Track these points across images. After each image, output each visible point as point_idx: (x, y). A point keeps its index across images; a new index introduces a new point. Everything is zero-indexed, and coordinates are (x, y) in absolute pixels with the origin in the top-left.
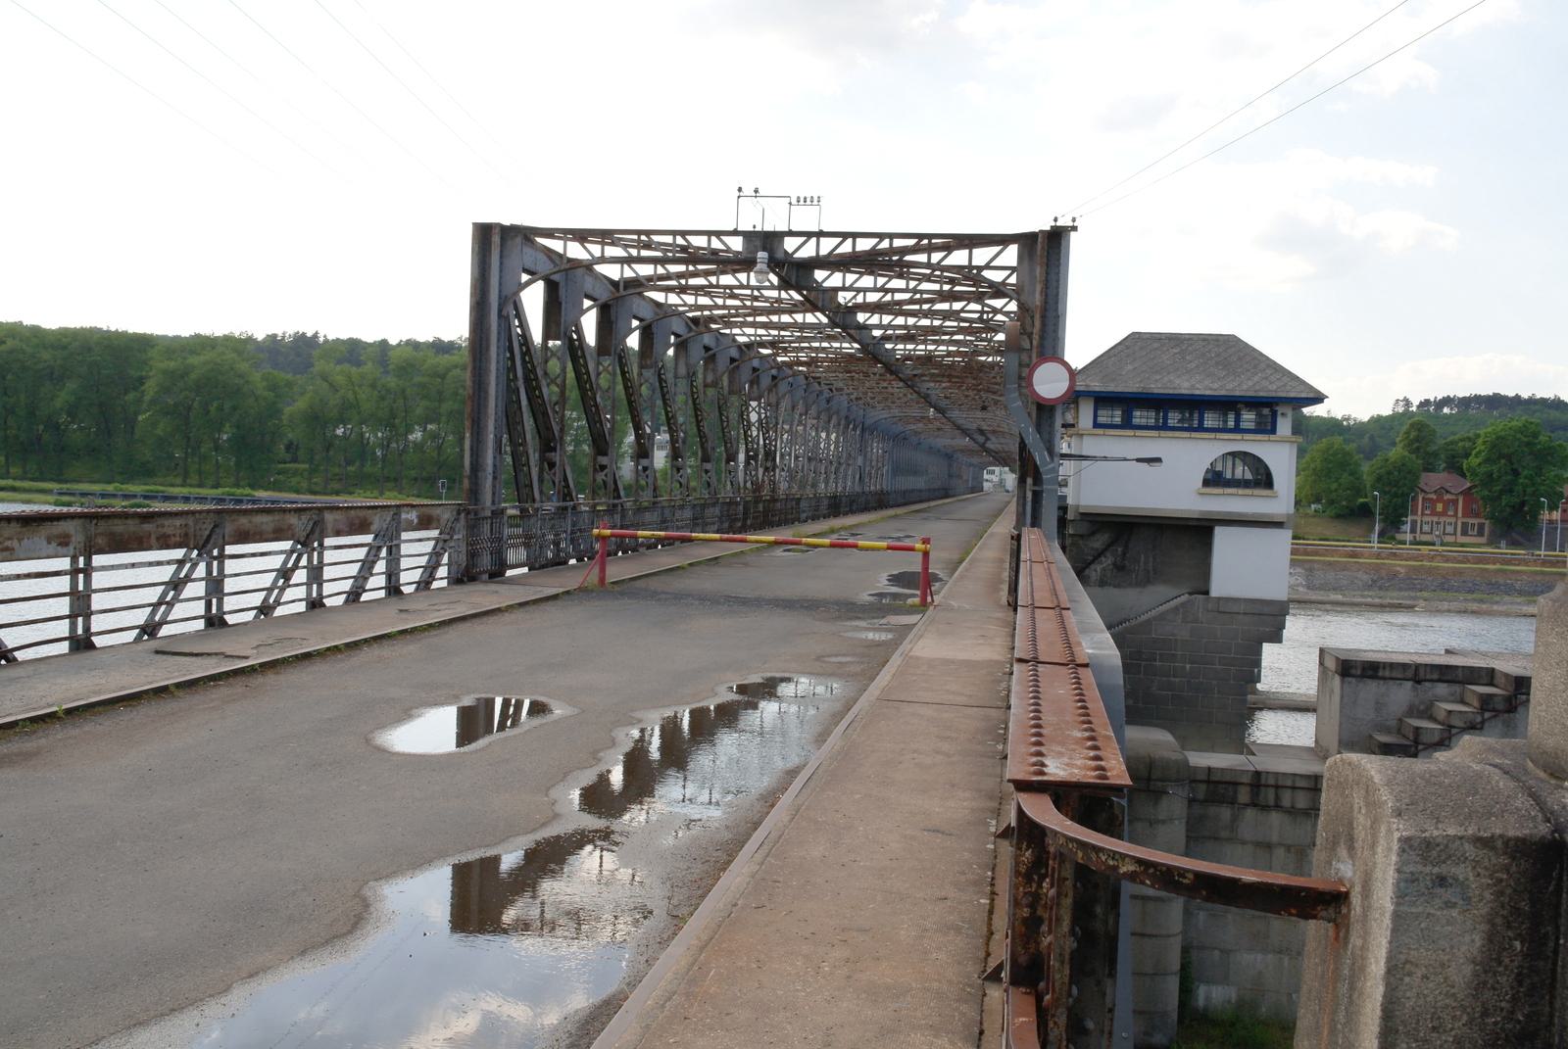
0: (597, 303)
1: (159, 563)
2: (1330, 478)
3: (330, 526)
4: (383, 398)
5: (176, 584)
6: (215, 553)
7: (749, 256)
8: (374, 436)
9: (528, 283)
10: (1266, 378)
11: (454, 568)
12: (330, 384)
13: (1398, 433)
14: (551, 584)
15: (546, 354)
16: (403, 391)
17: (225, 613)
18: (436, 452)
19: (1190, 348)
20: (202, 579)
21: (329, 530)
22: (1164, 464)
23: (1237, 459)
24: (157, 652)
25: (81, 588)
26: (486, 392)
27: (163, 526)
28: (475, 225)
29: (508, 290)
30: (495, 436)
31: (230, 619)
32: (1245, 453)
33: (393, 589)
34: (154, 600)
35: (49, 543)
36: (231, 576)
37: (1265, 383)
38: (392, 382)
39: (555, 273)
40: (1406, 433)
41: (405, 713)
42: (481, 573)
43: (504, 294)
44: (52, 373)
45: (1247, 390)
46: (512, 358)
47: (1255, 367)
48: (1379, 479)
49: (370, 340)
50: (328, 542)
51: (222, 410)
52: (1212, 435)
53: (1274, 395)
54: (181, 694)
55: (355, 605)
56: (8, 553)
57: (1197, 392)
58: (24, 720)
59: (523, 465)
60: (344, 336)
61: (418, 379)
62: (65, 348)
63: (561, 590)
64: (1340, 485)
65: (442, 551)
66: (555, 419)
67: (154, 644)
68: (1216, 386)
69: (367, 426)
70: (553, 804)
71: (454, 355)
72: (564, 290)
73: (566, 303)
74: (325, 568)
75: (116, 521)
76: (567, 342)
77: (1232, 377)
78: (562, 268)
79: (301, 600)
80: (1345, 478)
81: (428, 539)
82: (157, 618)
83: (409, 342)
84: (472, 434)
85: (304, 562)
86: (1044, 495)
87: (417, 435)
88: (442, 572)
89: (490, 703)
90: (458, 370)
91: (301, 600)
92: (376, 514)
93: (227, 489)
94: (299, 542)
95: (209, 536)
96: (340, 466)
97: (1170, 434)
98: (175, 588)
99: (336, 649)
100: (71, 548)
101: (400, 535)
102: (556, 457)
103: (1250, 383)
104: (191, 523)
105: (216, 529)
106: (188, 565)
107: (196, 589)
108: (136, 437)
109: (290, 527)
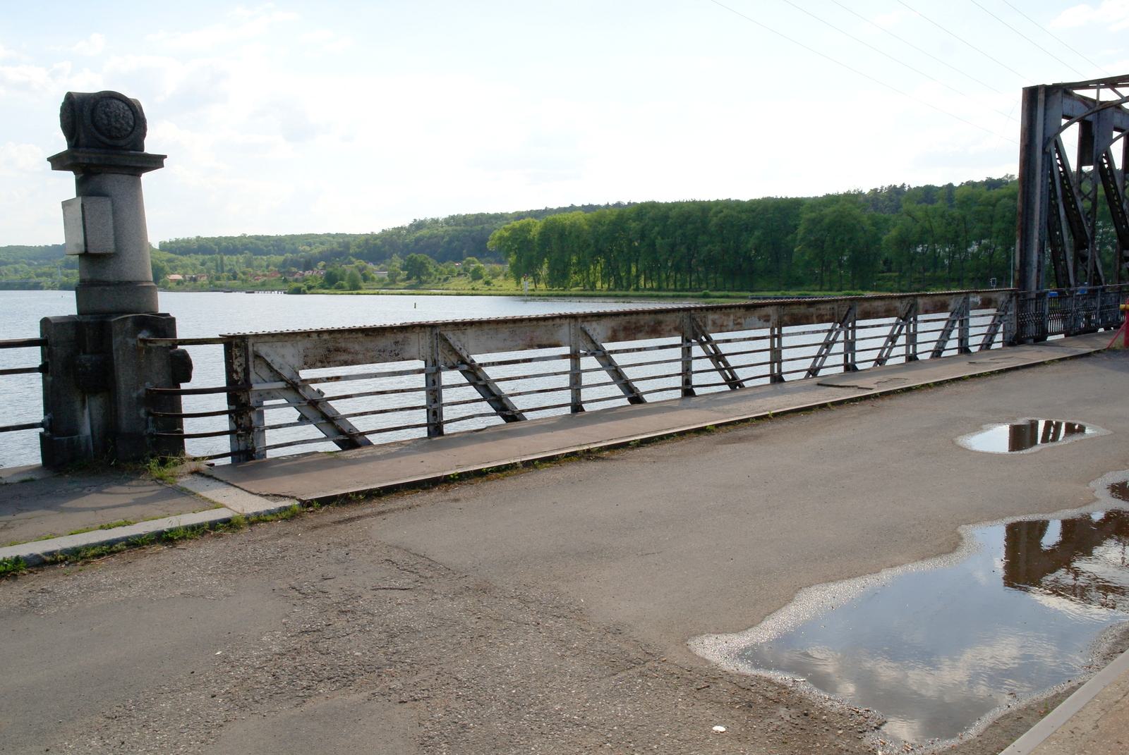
0: (1124, 133)
1: (818, 332)
3: (921, 307)
4: (949, 224)
5: (828, 345)
6: (850, 325)
8: (943, 251)
9: (1066, 126)
11: (1007, 335)
12: (913, 218)
14: (1083, 347)
15: (1081, 176)
16: (964, 218)
17: (856, 363)
18: (988, 259)
20: (843, 342)
21: (921, 310)
24: (819, 384)
25: (776, 346)
26: (1033, 210)
27: (820, 309)
28: (1025, 89)
29: (1050, 134)
30: (1039, 240)
31: (859, 366)
33: (964, 349)
34: (815, 354)
35: (760, 320)
36: (860, 339)
38: (956, 212)
39: (1089, 115)
41: (977, 427)
42: (1028, 338)
43: (1046, 136)
44: (747, 228)
46: (1053, 183)
49: (940, 185)
50: (920, 318)
51: (844, 241)
54: (835, 408)
55: (938, 360)
56: (738, 326)
58: (752, 418)
59: (1061, 260)
60: (922, 185)
61: (975, 208)
62: (753, 211)
63: (1093, 350)
65: (999, 323)
66: (1087, 224)
67: (816, 380)
69: (938, 245)
70: (1093, 492)
71: (1002, 188)
72: (1096, 127)
73: (1098, 136)
74: (918, 335)
75: (795, 307)
76: (1098, 166)
78: (1095, 109)
79: (902, 355)
81: (989, 315)
82: (817, 365)
83: (968, 183)
84: (1021, 240)
85: (904, 331)
87: (974, 248)
88: (999, 337)
89: (1034, 425)
90: (1006, 199)
91: (902, 355)
92: (952, 299)
93: (847, 291)
94: (901, 318)
95: (847, 315)
96: (919, 273)
98: (827, 347)
99: (927, 386)
100: (771, 323)
101: (969, 313)
102: (1088, 252)
104: (836, 307)
105: (851, 311)
106: (834, 333)
107: (839, 347)
108: (793, 262)
109: (895, 309)
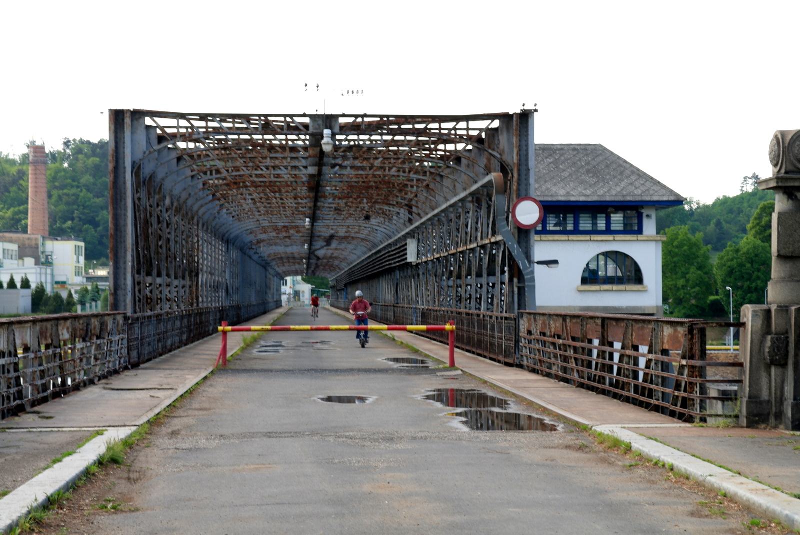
2: (676, 273)
7: (314, 131)
10: (631, 184)
13: (749, 217)
19: (563, 158)
22: (560, 265)
23: (608, 259)
32: (616, 253)
37: (631, 188)
40: (756, 219)
45: (616, 195)
47: (621, 173)
48: (731, 272)
52: (587, 237)
53: (638, 198)
57: (572, 199)
64: (687, 281)
68: (588, 192)
77: (601, 184)
80: (694, 274)
86: (526, 289)
97: (550, 237)
103: (618, 189)
